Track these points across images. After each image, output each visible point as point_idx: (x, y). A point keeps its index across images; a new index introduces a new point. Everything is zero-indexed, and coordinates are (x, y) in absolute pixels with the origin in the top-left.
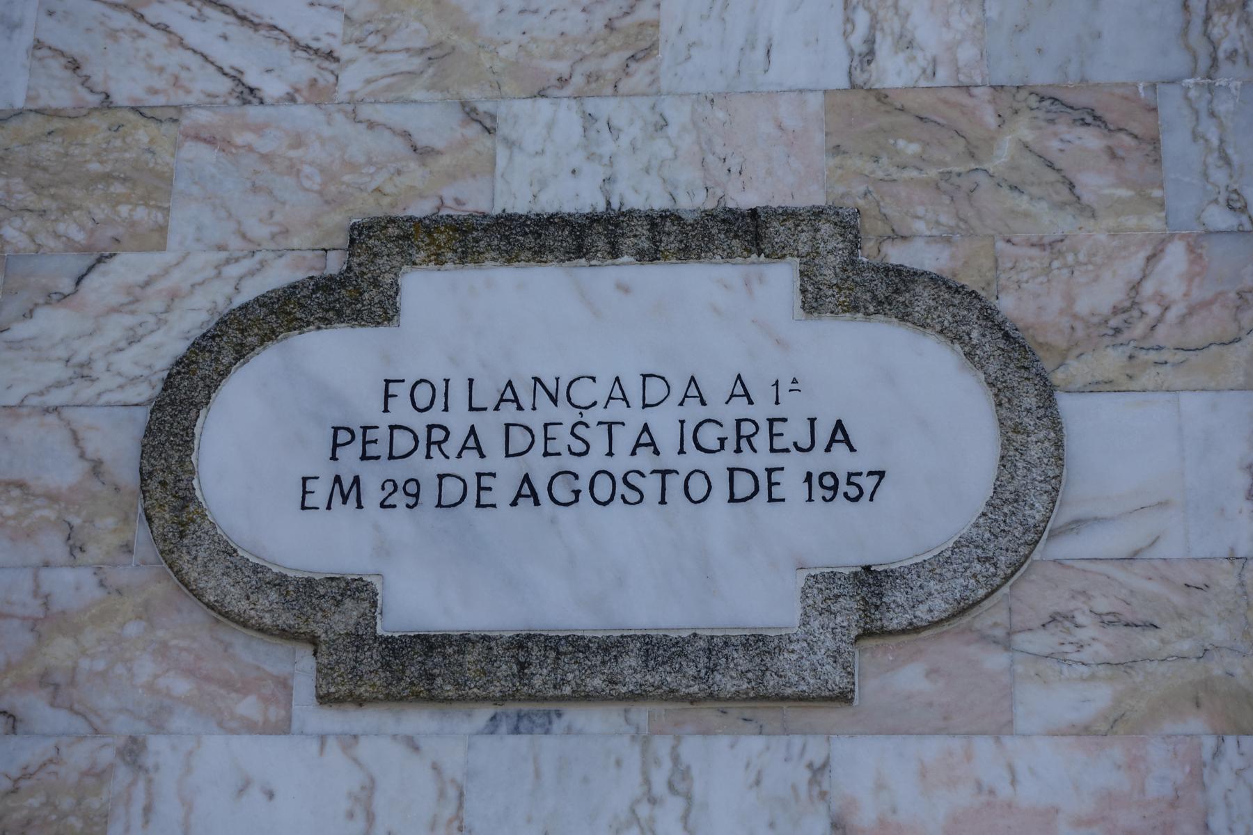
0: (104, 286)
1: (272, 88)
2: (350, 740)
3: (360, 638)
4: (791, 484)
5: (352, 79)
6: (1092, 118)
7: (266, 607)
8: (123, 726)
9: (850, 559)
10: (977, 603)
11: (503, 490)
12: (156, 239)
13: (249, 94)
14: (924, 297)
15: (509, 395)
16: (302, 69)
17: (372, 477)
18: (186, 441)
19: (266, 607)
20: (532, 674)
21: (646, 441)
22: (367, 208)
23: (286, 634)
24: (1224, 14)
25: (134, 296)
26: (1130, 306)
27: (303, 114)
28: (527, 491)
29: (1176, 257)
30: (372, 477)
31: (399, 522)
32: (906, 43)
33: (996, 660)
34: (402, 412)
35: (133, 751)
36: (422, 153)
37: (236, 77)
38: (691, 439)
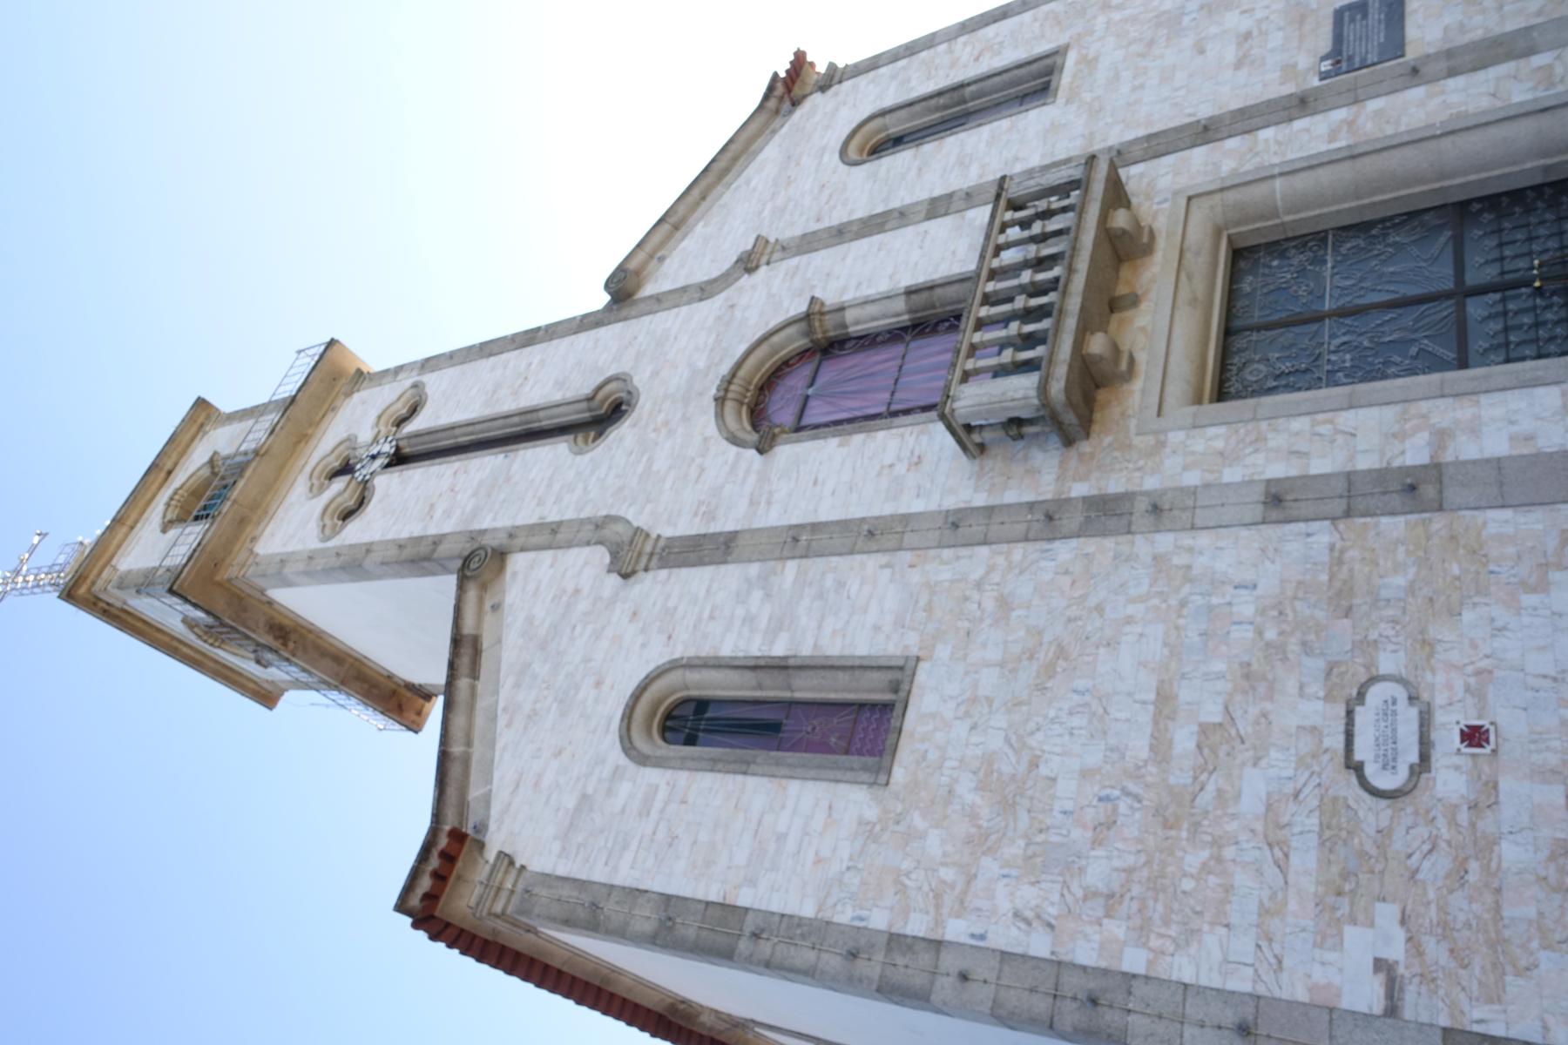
0: (1354, 805)
1: (1318, 781)
2: (1437, 769)
3: (1420, 765)
4: (1394, 708)
5: (1316, 768)
6: (1331, 669)
7: (1414, 779)
8: (1435, 801)
9: (1406, 701)
10: (1281, 174)
11: (1394, 746)
12: (1346, 799)
13: (1319, 785)
14: (1363, 690)
15: (1378, 745)
16: (1315, 777)
17: (1391, 764)
18: (1384, 791)
19: (1414, 779)
20: (1345, 582)
21: (1386, 727)
22: (1343, 765)
23: (1419, 777)
24: (1040, 400)
25: (1356, 801)
26: (1365, 666)
27: (1324, 776)
28: (1395, 743)
29: (1357, 660)
30: (1391, 764)
31: (1400, 760)
32: (1317, 692)
33: (1422, 685)
34: (1381, 760)
35: (1439, 800)
36: (1332, 759)
37: (1315, 787)
38: (1386, 721)
